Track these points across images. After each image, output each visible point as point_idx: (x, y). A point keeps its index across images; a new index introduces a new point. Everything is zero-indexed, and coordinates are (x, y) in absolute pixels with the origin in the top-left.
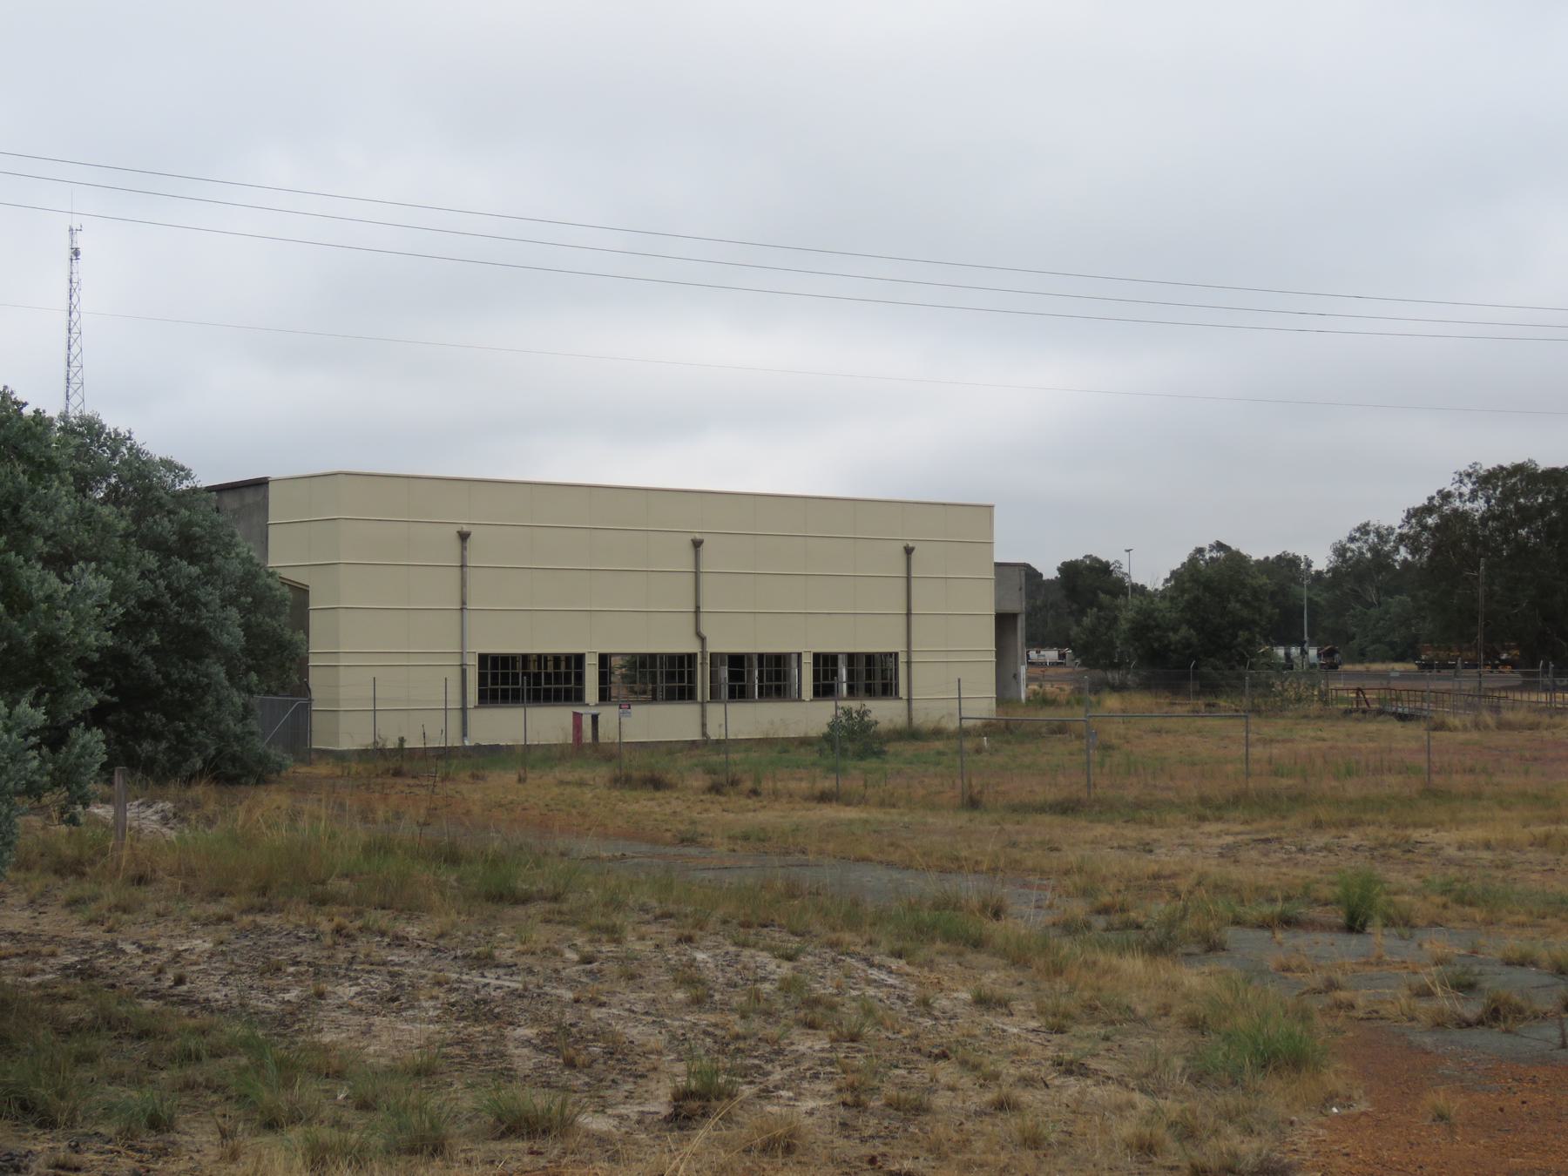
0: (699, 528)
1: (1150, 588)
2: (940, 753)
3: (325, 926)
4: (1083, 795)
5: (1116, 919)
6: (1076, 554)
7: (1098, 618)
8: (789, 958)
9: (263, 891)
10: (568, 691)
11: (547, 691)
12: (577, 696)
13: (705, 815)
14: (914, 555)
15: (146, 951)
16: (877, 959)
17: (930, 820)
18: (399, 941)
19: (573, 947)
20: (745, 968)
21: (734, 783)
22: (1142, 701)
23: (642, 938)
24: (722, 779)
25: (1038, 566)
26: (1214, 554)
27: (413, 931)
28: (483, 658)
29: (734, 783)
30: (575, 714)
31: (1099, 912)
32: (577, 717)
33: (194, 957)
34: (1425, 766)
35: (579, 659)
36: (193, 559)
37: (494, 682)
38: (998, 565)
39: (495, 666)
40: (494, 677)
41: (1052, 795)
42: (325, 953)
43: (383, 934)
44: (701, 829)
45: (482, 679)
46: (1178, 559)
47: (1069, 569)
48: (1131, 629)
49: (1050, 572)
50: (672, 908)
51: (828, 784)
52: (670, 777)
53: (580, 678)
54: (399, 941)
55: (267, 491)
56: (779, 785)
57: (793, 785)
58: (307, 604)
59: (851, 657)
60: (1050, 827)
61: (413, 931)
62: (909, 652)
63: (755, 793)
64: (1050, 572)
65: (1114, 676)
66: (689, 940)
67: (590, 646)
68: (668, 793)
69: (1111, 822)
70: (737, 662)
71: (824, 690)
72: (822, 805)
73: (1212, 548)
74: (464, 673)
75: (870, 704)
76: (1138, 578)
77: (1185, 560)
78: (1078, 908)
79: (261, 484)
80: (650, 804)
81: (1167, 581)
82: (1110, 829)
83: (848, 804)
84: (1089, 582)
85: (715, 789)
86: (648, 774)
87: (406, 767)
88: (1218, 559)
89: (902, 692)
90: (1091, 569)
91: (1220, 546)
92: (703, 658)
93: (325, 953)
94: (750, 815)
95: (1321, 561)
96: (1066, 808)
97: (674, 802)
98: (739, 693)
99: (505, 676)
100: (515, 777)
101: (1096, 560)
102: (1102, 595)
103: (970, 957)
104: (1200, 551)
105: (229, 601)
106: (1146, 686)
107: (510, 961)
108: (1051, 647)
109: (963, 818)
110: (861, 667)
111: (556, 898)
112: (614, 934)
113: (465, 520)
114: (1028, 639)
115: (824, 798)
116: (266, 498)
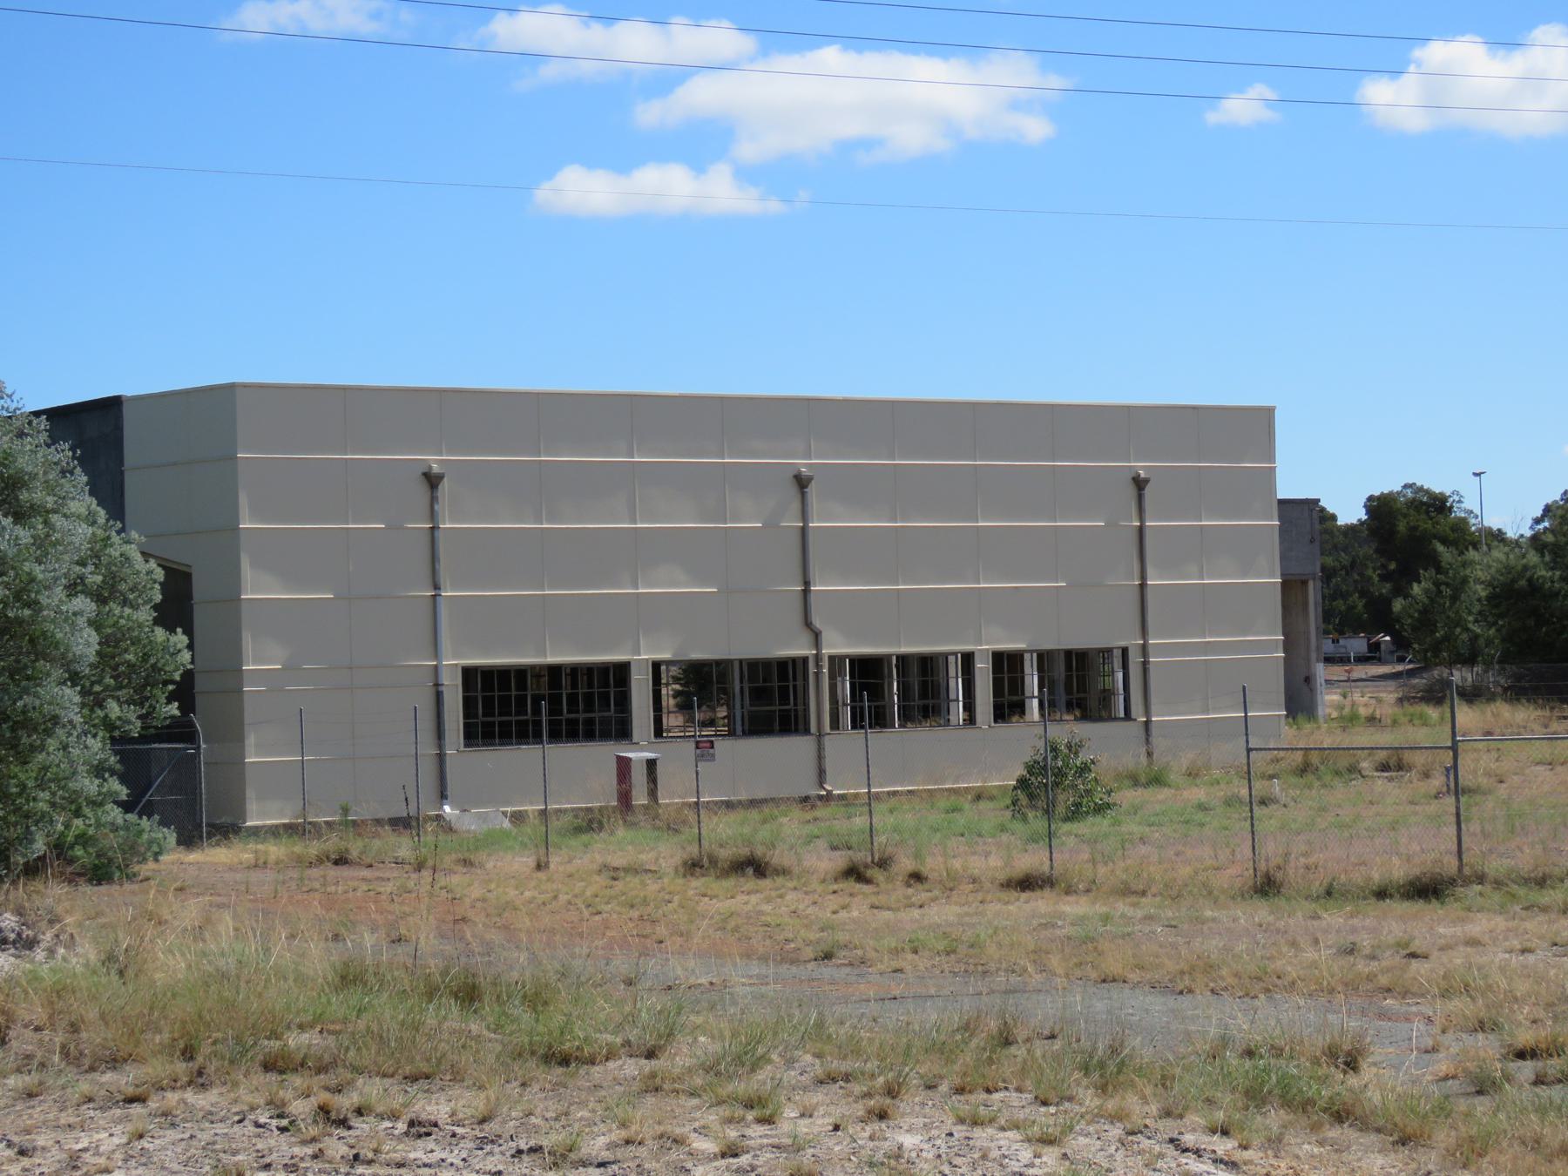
1: (1511, 534)
2: (1202, 807)
3: (300, 1108)
6: (1389, 484)
7: (1437, 584)
8: (1048, 1141)
9: (188, 1054)
10: (605, 722)
12: (623, 732)
13: (843, 914)
15: (22, 1152)
16: (1189, 1139)
18: (420, 1129)
19: (703, 1131)
20: (984, 1157)
21: (883, 863)
22: (1523, 715)
23: (806, 1114)
24: (862, 856)
25: (1329, 505)
27: (437, 1108)
28: (468, 673)
29: (883, 863)
31: (1521, 1055)
32: (624, 766)
33: (102, 1161)
37: (488, 711)
38: (1282, 502)
39: (488, 685)
40: (488, 703)
41: (1399, 871)
42: (309, 1150)
43: (394, 1116)
44: (842, 937)
45: (468, 704)
47: (1380, 507)
48: (1489, 598)
49: (1349, 512)
50: (836, 1065)
51: (1032, 860)
52: (778, 857)
54: (420, 1129)
55: (121, 411)
56: (957, 864)
57: (977, 865)
59: (1044, 658)
61: (437, 1108)
63: (917, 877)
64: (1349, 512)
65: (1460, 676)
66: (882, 1116)
67: (642, 654)
68: (780, 880)
69: (1502, 910)
70: (867, 671)
71: (1008, 707)
76: (1493, 520)
79: (111, 406)
80: (754, 899)
81: (1537, 521)
82: (1500, 922)
83: (1069, 891)
84: (1411, 531)
85: (854, 873)
86: (745, 852)
87: (355, 848)
89: (813, 729)
93: (309, 1150)
95: (1365, 517)
96: (1427, 889)
98: (871, 716)
99: (504, 702)
102: (1440, 548)
103: (1333, 1133)
106: (1517, 693)
107: (606, 1155)
108: (1356, 632)
109: (1262, 911)
110: (1060, 670)
111: (651, 1054)
112: (762, 1109)
113: (432, 451)
114: (1327, 616)
115: (1026, 884)
116: (119, 428)
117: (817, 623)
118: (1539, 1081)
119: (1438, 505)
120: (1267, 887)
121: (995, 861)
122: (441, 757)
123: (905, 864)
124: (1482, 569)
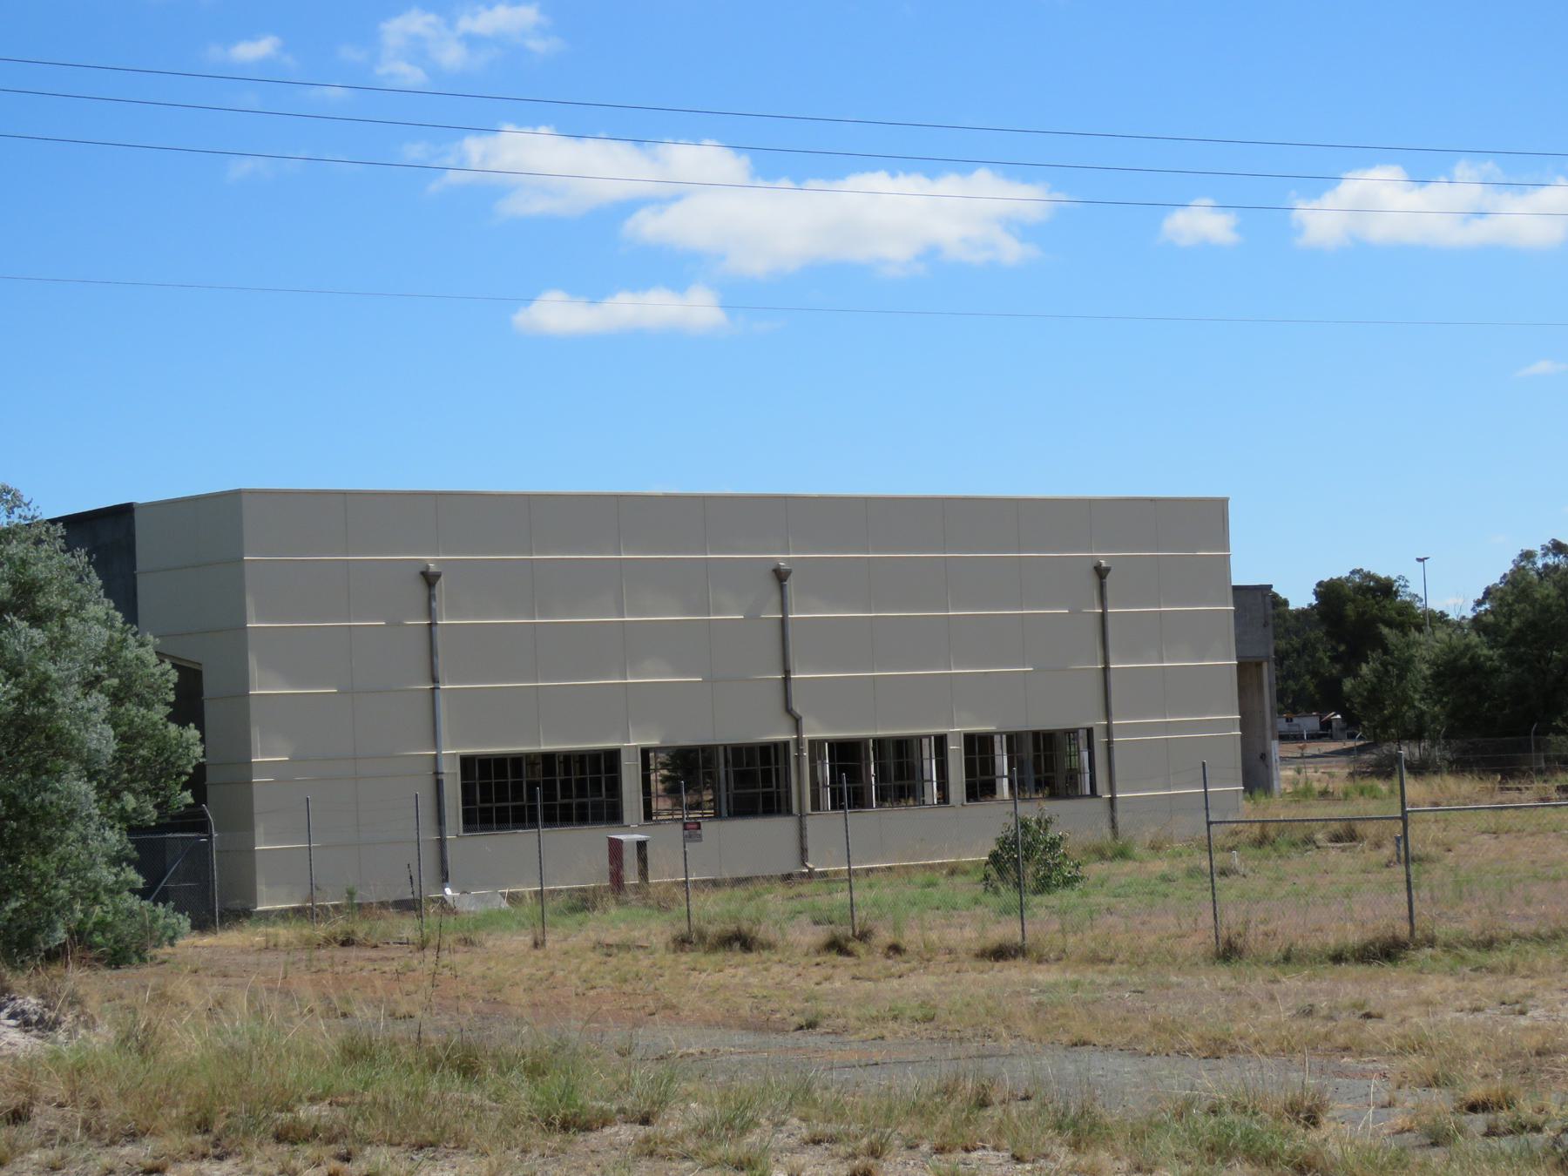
0: (779, 546)
1: (1453, 616)
2: (1165, 879)
4: (1403, 930)
5: (1504, 1117)
6: (1338, 569)
11: (567, 807)
12: (614, 815)
13: (826, 986)
14: (1109, 580)
17: (1039, 977)
21: (864, 936)
22: (1464, 787)
24: (843, 930)
26: (1551, 560)
29: (864, 936)
30: (612, 841)
31: (1473, 1108)
32: (616, 848)
34: (1216, 879)
35: (613, 756)
36: (37, 620)
38: (1236, 588)
39: (485, 773)
40: (485, 790)
46: (1495, 570)
47: (1329, 593)
49: (1300, 597)
50: (821, 1128)
51: (1005, 931)
52: (764, 932)
53: (615, 786)
57: (953, 937)
58: (200, 693)
59: (1013, 739)
60: (1353, 984)
62: (1108, 730)
63: (895, 949)
64: (1300, 597)
68: (765, 954)
70: (846, 754)
71: (981, 788)
72: (998, 965)
73: (1546, 551)
74: (438, 784)
75: (1052, 807)
76: (1435, 605)
77: (1508, 567)
78: (1440, 1101)
79: (123, 513)
81: (1479, 603)
82: (1451, 983)
83: (1041, 960)
84: (1359, 614)
85: (836, 946)
86: (732, 927)
87: (361, 929)
88: (1556, 567)
89: (795, 810)
90: (1362, 590)
91: (1359, 571)
92: (799, 750)
94: (895, 983)
97: (776, 969)
98: (850, 797)
99: (501, 789)
100: (529, 940)
101: (1369, 576)
102: (1385, 630)
104: (1528, 555)
105: (91, 683)
106: (1461, 766)
108: (1308, 712)
111: (645, 1121)
114: (1281, 696)
115: (1000, 953)
117: (797, 708)
118: (1491, 1132)
119: (1385, 589)
120: (1228, 952)
121: (969, 933)
122: (442, 842)
123: (884, 936)
124: (1426, 649)
